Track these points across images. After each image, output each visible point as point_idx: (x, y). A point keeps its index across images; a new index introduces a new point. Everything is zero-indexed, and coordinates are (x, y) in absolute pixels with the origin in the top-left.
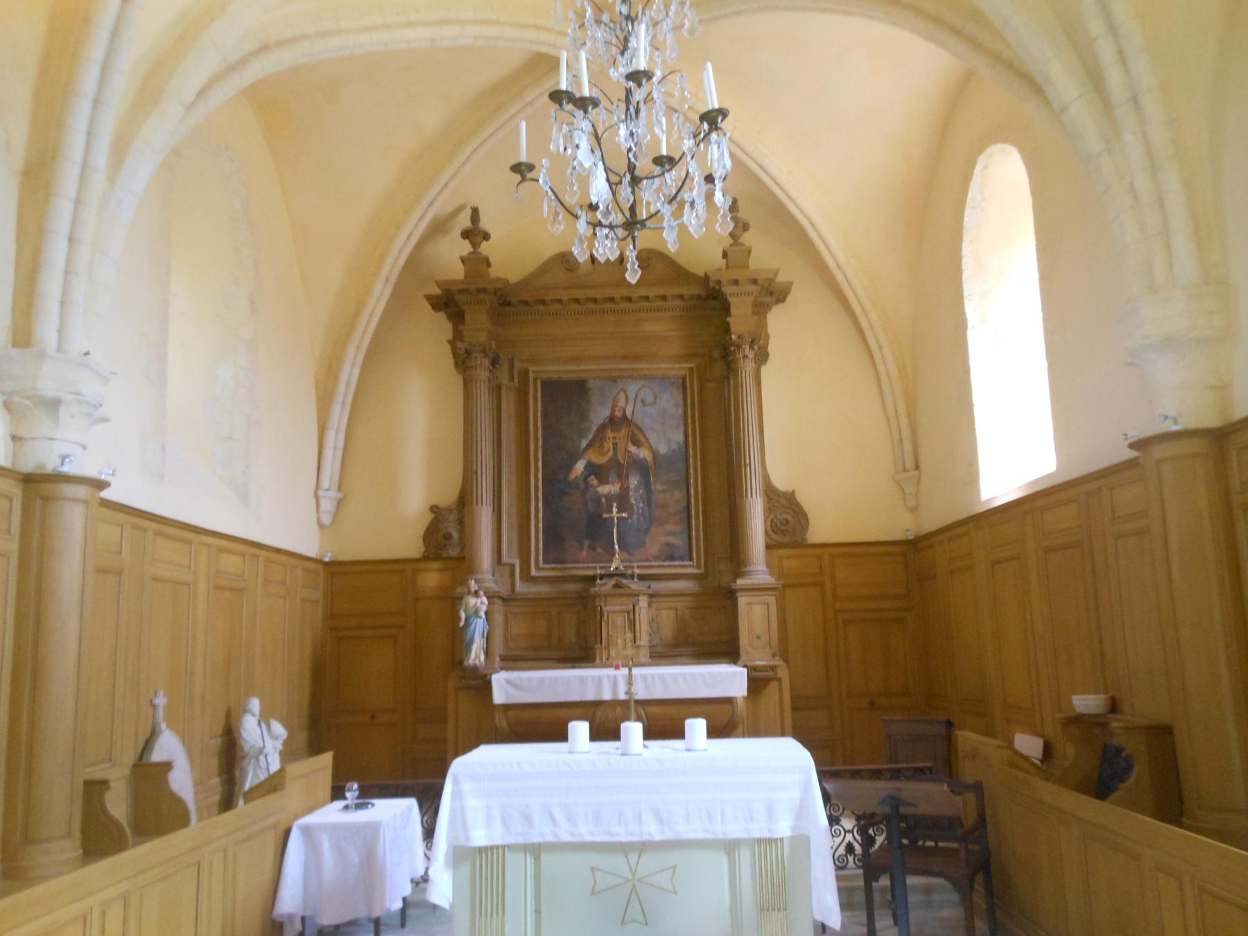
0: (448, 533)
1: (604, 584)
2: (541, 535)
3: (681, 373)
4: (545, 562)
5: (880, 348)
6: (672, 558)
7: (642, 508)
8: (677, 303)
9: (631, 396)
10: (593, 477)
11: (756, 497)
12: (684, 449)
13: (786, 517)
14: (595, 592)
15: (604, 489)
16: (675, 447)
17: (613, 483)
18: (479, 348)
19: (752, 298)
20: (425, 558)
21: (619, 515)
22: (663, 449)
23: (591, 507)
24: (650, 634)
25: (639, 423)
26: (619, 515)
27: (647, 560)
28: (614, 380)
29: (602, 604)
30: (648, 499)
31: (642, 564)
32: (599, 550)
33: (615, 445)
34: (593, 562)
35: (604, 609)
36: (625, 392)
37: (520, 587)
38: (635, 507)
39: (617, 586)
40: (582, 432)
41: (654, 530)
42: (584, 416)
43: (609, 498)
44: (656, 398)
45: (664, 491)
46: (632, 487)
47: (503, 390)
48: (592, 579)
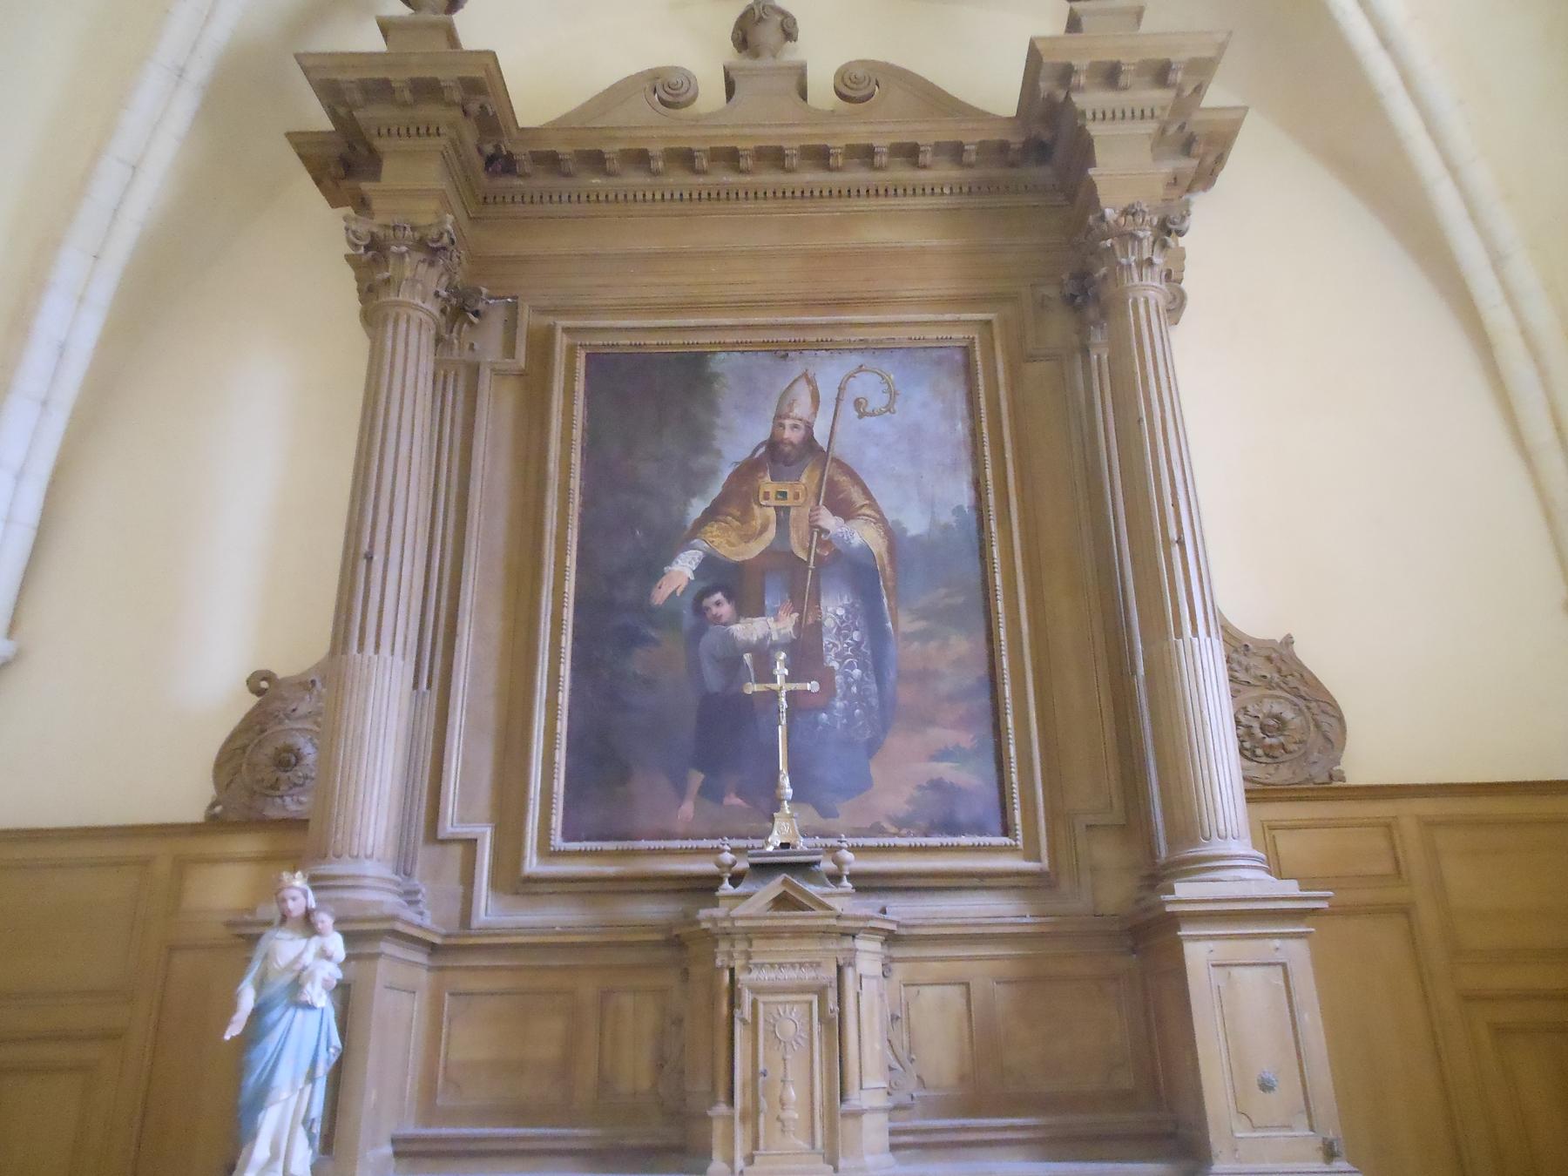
0: (289, 749)
1: (747, 896)
2: (561, 756)
3: (958, 334)
4: (567, 836)
5: (1497, 261)
6: (950, 826)
7: (860, 682)
8: (943, 172)
9: (827, 393)
10: (719, 596)
11: (1209, 634)
12: (974, 525)
13: (1276, 709)
14: (714, 920)
15: (750, 630)
16: (947, 518)
17: (775, 613)
18: (408, 232)
19: (1151, 127)
20: (216, 823)
21: (792, 686)
22: (915, 523)
23: (714, 680)
24: (891, 1069)
25: (849, 460)
26: (792, 686)
27: (878, 831)
28: (781, 352)
29: (738, 963)
30: (876, 653)
31: (861, 842)
32: (733, 800)
33: (783, 513)
34: (714, 837)
35: (742, 977)
36: (810, 381)
37: (488, 910)
38: (838, 678)
39: (782, 902)
40: (693, 482)
41: (896, 743)
42: (700, 439)
43: (763, 654)
44: (893, 395)
45: (925, 636)
46: (829, 623)
47: (486, 378)
48: (704, 887)
